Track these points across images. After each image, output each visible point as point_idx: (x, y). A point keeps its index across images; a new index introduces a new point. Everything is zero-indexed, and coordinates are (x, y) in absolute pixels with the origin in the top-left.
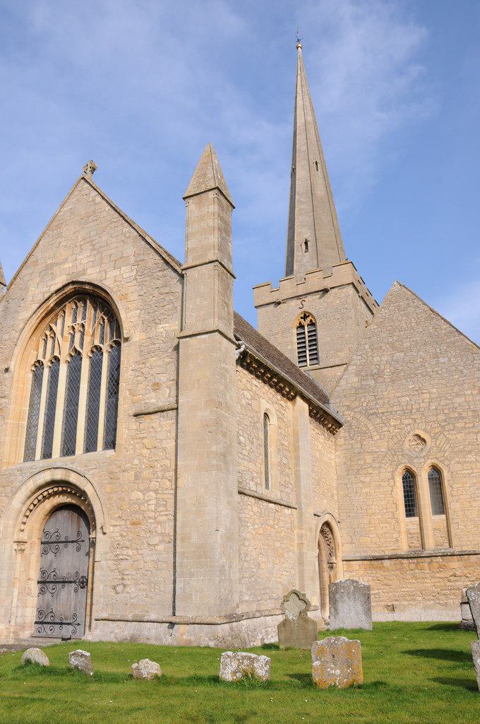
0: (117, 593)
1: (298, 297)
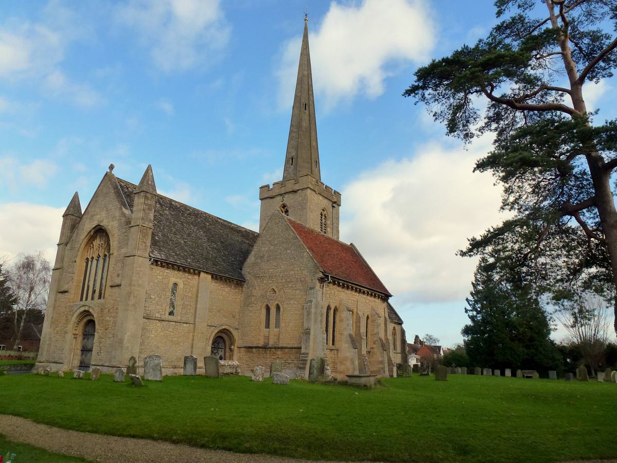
0: (98, 355)
1: (281, 195)
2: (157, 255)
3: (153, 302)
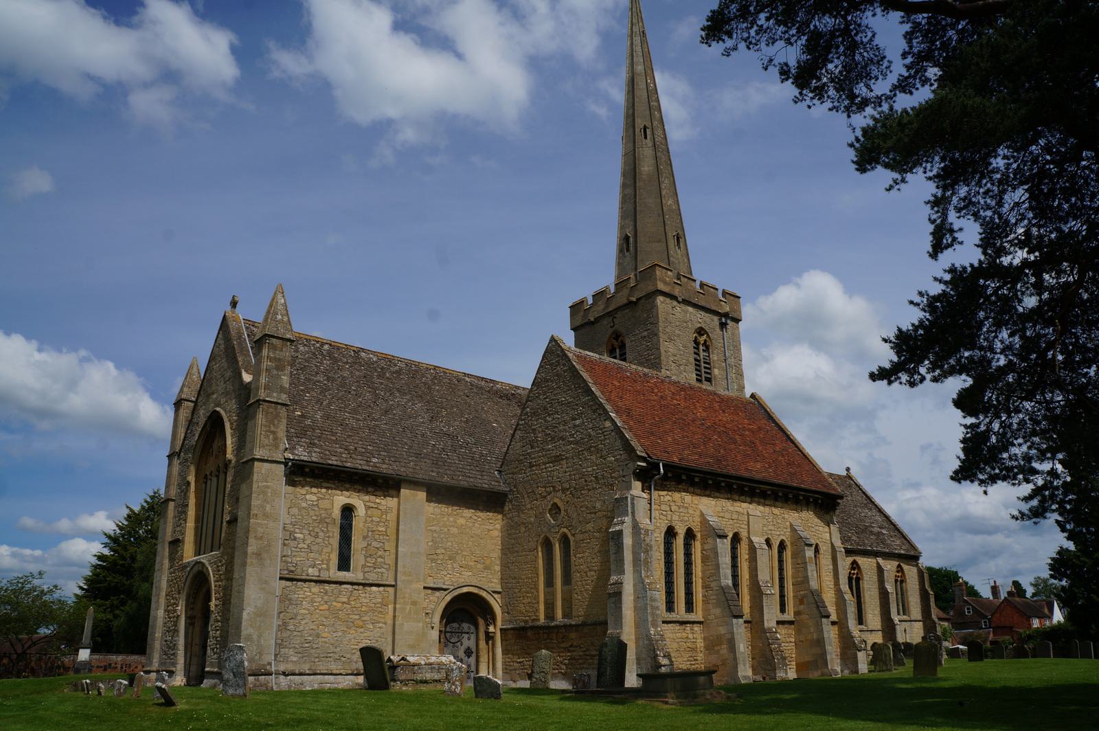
2: (302, 454)
3: (301, 545)
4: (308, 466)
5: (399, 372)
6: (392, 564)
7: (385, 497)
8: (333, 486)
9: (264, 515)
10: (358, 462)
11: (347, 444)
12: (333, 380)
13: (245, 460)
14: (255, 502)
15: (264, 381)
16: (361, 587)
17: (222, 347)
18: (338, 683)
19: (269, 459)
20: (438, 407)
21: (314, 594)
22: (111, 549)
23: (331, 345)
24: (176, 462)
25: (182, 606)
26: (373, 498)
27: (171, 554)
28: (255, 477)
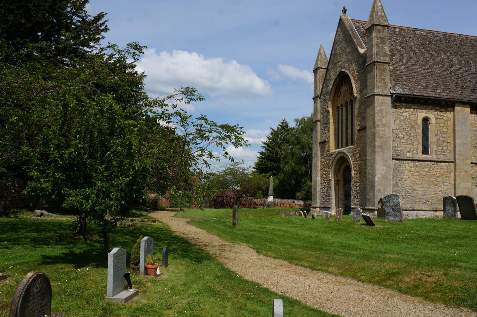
2: (399, 90)
3: (402, 141)
4: (404, 97)
5: (440, 40)
6: (452, 149)
7: (446, 112)
8: (417, 107)
9: (382, 125)
10: (430, 93)
11: (422, 83)
12: (405, 48)
13: (368, 95)
14: (377, 118)
15: (375, 51)
16: (436, 163)
17: (341, 36)
18: (426, 215)
19: (383, 94)
20: (467, 58)
21: (410, 167)
22: (266, 149)
23: (399, 29)
24: (319, 101)
25: (332, 175)
26: (439, 113)
27: (321, 149)
28: (376, 105)
